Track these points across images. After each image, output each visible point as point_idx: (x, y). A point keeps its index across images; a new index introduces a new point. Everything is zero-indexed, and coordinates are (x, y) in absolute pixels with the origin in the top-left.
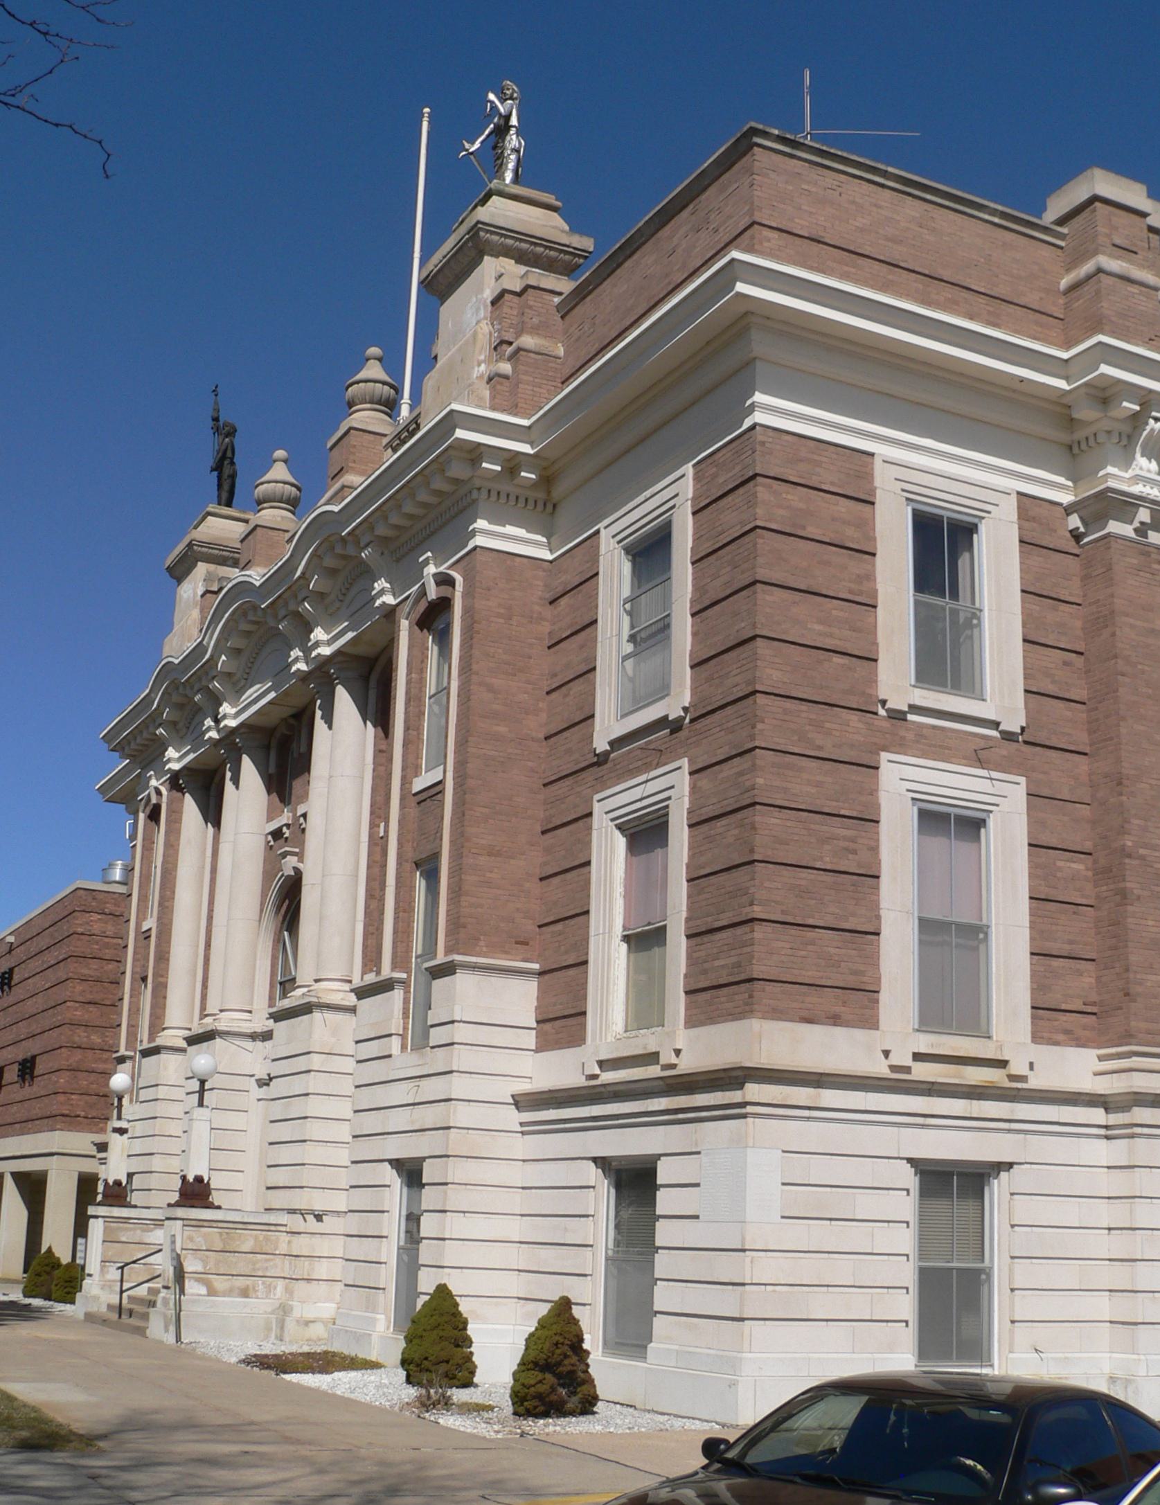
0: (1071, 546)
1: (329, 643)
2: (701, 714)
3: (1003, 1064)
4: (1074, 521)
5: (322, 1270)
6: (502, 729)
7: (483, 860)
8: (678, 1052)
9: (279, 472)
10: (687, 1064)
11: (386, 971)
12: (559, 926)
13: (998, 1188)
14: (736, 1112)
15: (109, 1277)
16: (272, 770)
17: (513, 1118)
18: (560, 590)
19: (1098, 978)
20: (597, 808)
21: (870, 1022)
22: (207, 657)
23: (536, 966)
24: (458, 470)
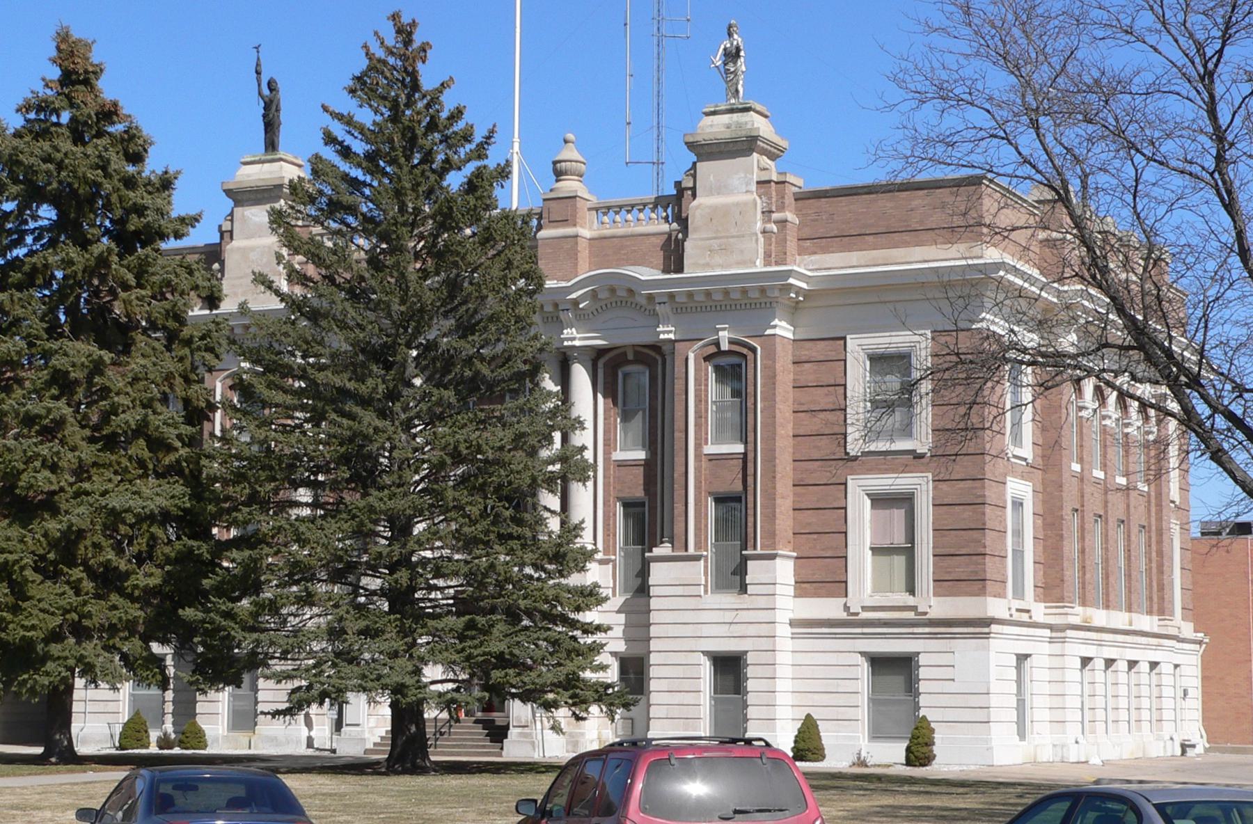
1: (580, 339)
3: (1028, 611)
10: (934, 614)
12: (815, 536)
14: (986, 636)
18: (804, 358)
20: (850, 483)
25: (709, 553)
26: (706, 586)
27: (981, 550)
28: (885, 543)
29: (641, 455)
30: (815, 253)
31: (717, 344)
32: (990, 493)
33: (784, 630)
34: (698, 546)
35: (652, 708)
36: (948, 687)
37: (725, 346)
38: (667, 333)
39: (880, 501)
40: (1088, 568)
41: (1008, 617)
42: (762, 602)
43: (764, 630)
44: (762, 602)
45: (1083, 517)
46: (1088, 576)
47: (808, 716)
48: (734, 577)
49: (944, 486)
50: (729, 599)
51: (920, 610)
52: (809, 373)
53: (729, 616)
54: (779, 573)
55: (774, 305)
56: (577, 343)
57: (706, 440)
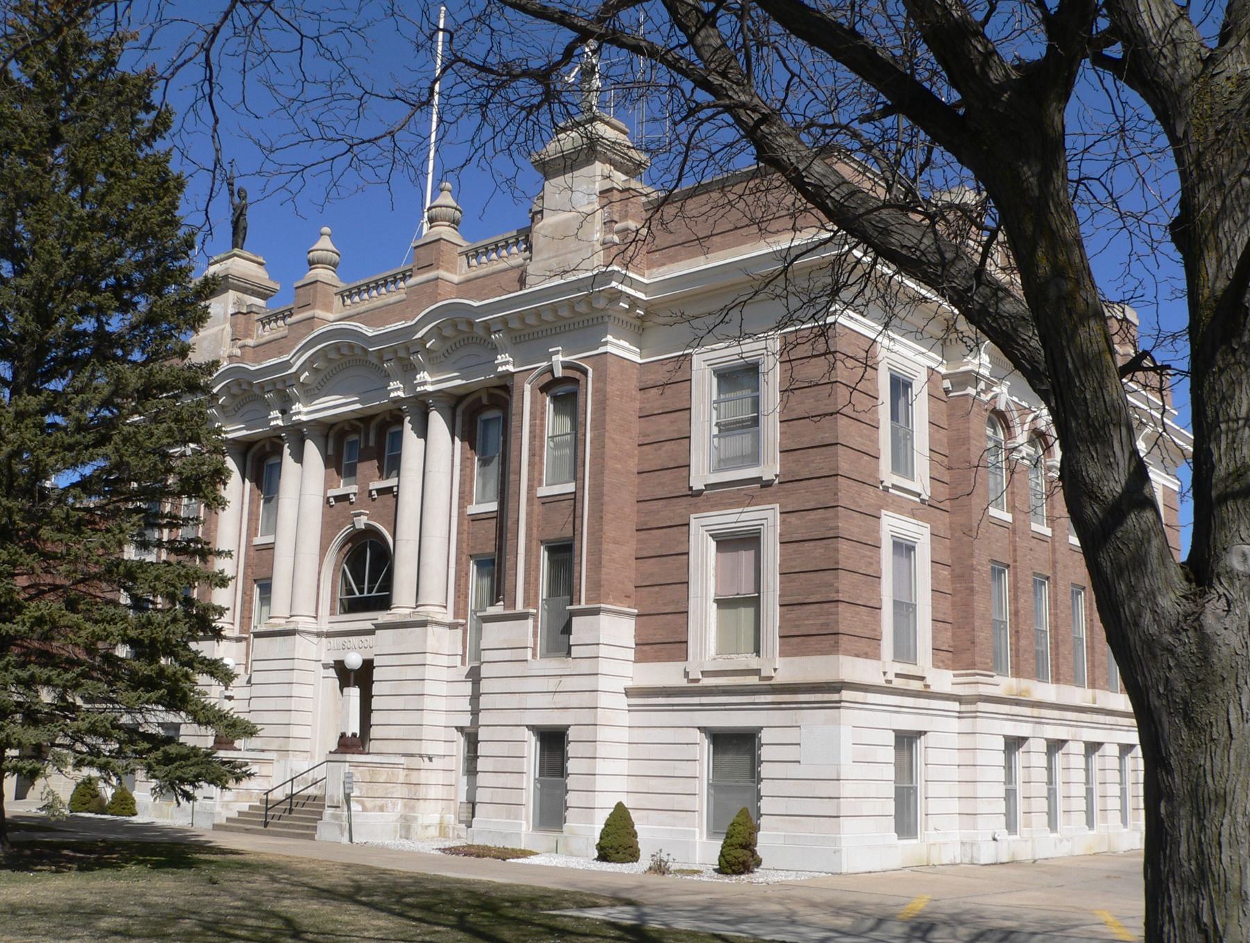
0: (943, 396)
1: (433, 383)
2: (788, 481)
3: (922, 678)
4: (947, 384)
5: (433, 792)
6: (619, 466)
7: (611, 546)
8: (775, 670)
9: (325, 243)
10: (780, 678)
11: (520, 607)
12: (657, 589)
13: (921, 743)
14: (836, 705)
15: (226, 799)
16: (330, 452)
17: (624, 701)
18: (650, 383)
19: (953, 634)
20: (693, 523)
21: (876, 656)
22: (290, 371)
23: (636, 611)
24: (601, 304)
25: (540, 611)
26: (534, 649)
27: (833, 596)
28: (730, 593)
29: (493, 506)
30: (663, 264)
31: (550, 370)
32: (848, 525)
33: (613, 702)
34: (527, 603)
35: (479, 791)
36: (793, 771)
37: (559, 373)
38: (506, 363)
39: (728, 542)
40: (1023, 634)
41: (883, 683)
42: (584, 667)
43: (585, 699)
44: (584, 667)
45: (1015, 575)
46: (1023, 642)
47: (620, 806)
48: (560, 639)
49: (793, 519)
50: (554, 665)
51: (763, 674)
52: (654, 400)
53: (551, 684)
54: (612, 633)
55: (606, 319)
56: (430, 388)
57: (541, 478)
